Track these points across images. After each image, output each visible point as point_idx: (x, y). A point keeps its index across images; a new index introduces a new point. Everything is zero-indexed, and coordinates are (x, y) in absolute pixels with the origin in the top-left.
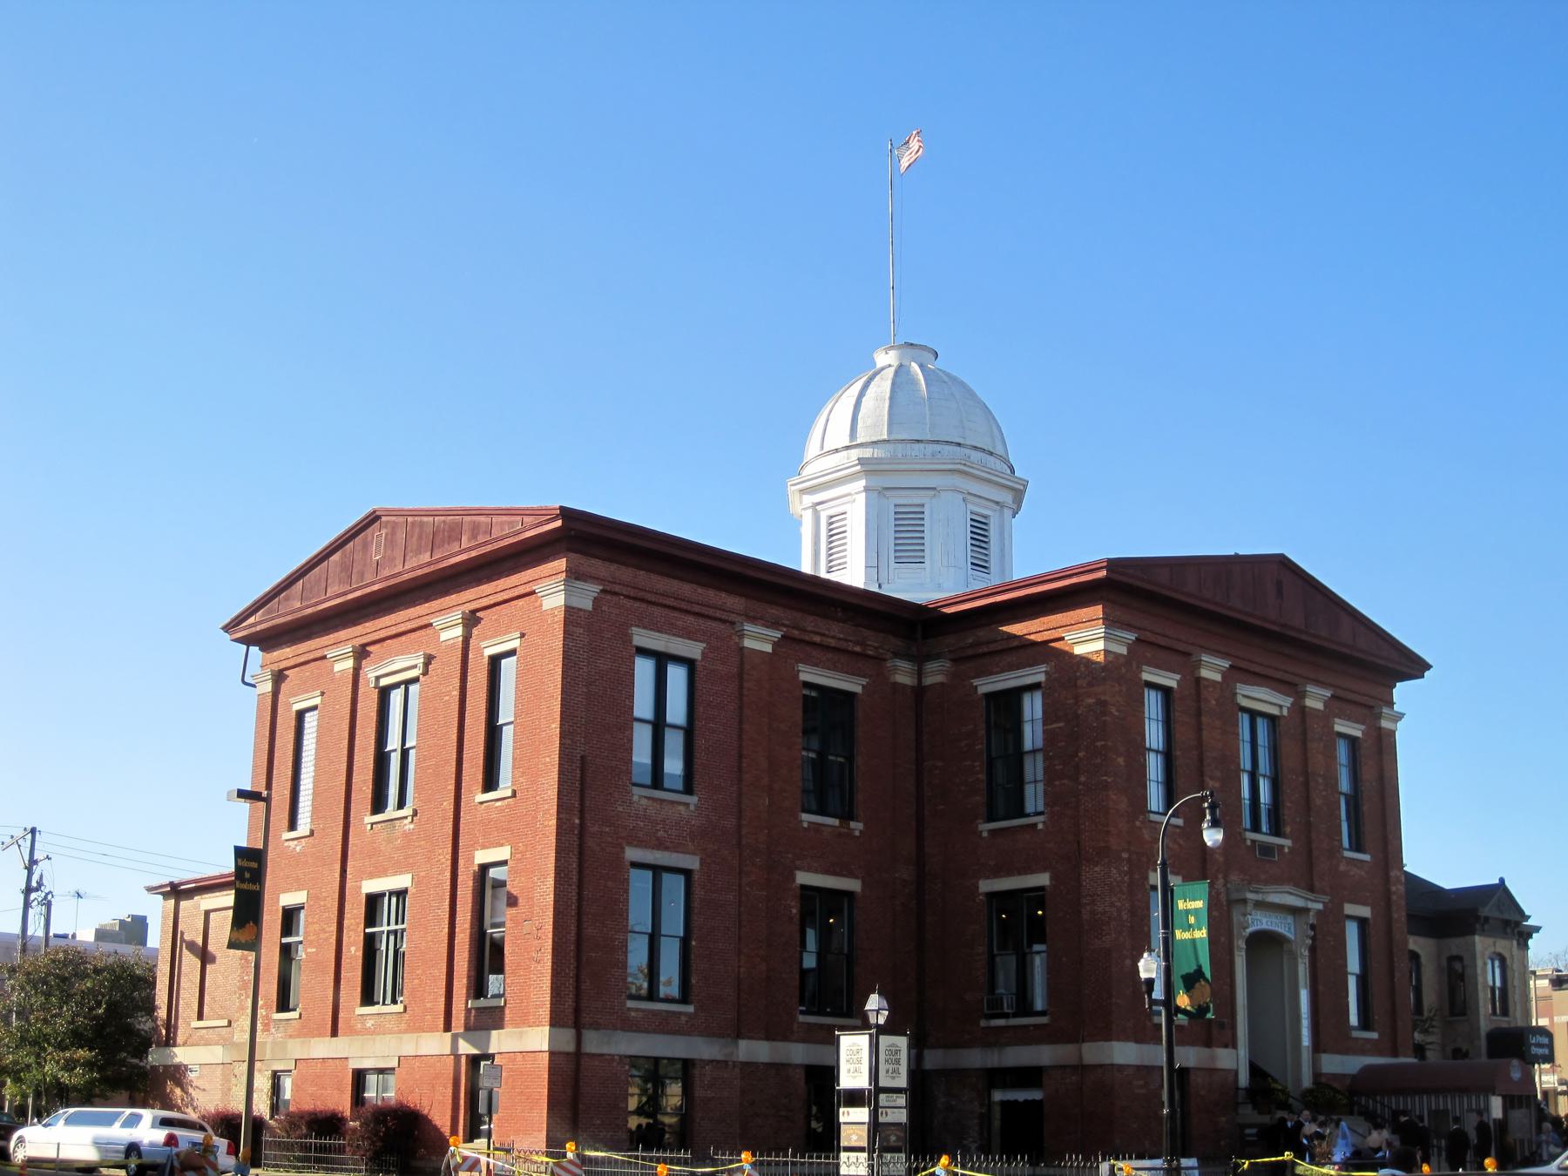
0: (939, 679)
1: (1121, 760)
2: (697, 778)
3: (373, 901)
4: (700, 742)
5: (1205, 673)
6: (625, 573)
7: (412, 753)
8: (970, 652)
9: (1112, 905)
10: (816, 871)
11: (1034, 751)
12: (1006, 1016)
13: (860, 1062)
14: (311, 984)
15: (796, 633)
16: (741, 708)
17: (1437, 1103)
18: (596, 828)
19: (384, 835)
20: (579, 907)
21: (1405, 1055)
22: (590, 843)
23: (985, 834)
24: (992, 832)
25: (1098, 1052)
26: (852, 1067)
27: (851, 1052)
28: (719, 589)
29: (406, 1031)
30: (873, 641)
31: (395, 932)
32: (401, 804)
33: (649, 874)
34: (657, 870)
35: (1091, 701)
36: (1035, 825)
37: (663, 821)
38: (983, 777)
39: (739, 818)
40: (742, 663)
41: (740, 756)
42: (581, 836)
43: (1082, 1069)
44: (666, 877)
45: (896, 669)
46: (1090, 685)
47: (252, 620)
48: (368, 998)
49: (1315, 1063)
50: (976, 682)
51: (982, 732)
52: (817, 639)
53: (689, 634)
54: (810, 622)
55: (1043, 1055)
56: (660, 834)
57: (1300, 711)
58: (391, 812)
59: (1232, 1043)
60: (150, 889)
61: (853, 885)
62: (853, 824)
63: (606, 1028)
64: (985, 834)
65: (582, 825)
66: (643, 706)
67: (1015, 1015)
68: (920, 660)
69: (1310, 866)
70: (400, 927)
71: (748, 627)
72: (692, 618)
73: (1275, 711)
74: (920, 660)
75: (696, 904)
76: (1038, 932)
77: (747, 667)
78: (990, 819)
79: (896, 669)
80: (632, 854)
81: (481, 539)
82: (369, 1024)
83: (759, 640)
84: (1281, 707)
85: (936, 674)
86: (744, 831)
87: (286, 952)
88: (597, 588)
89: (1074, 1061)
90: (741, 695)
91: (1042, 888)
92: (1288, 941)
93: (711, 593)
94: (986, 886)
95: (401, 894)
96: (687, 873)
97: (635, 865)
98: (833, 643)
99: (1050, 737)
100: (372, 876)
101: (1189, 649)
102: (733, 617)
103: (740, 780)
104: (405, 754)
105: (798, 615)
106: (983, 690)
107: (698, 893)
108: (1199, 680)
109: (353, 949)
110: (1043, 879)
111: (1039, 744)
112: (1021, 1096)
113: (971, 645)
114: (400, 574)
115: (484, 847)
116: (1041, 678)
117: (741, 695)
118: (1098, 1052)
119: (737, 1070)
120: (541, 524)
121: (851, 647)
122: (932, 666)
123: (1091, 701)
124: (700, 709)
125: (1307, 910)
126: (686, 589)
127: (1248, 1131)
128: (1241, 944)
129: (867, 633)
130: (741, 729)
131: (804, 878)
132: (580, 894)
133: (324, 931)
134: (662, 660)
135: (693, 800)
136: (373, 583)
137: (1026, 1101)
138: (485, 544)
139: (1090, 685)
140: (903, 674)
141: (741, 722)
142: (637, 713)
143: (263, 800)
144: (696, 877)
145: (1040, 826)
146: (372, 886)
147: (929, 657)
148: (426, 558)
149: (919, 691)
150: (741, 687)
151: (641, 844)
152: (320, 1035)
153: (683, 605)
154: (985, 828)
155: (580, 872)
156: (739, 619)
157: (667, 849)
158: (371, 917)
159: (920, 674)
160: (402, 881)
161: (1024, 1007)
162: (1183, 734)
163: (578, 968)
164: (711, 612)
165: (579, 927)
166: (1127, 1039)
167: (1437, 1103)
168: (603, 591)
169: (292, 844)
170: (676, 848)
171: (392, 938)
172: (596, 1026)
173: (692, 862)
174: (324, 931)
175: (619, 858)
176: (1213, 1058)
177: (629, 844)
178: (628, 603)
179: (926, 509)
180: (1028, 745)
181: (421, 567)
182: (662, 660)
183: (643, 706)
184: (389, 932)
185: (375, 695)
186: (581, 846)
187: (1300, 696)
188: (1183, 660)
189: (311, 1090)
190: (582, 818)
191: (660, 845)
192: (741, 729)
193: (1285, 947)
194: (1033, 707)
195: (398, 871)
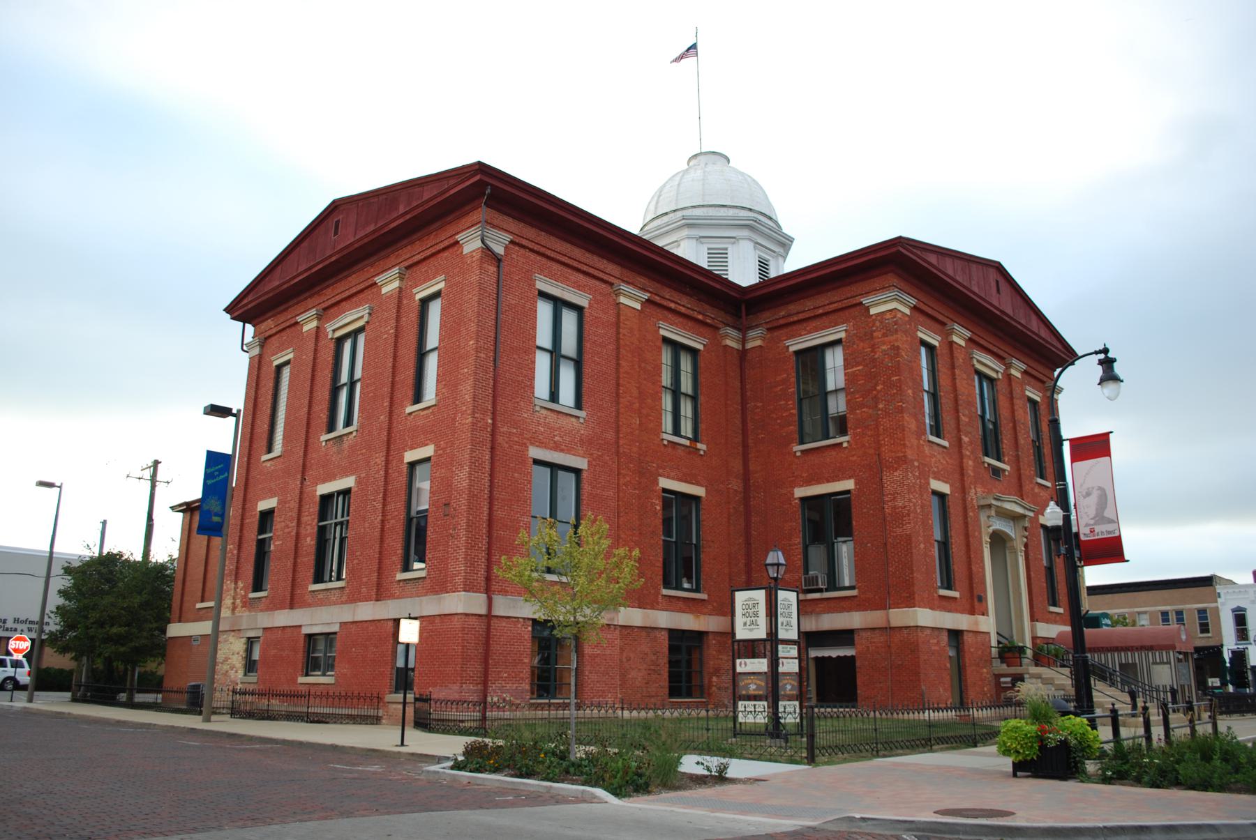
0: (758, 343)
1: (910, 392)
2: (585, 399)
3: (326, 499)
4: (587, 370)
5: (955, 339)
6: (530, 232)
7: (358, 386)
8: (782, 322)
9: (910, 501)
10: (673, 479)
11: (836, 391)
12: (820, 590)
13: (756, 615)
14: (276, 569)
15: (657, 299)
16: (618, 348)
17: (1127, 658)
18: (505, 429)
19: (334, 449)
20: (491, 492)
21: (1190, 610)
22: (500, 439)
23: (798, 454)
24: (802, 451)
25: (900, 616)
26: (748, 620)
27: (746, 606)
28: (603, 257)
29: (346, 602)
30: (712, 314)
31: (341, 523)
32: (348, 422)
33: (548, 470)
34: (554, 467)
35: (884, 347)
36: (841, 444)
37: (559, 428)
38: (795, 411)
39: (618, 432)
40: (618, 315)
41: (618, 385)
42: (493, 434)
43: (889, 630)
44: (561, 474)
45: (727, 335)
46: (885, 335)
47: (245, 301)
48: (319, 579)
49: (1033, 630)
50: (788, 343)
51: (794, 380)
52: (672, 305)
53: (578, 286)
54: (667, 293)
55: (853, 620)
56: (557, 438)
57: (1009, 377)
58: (340, 429)
59: (984, 613)
60: (172, 508)
61: (699, 491)
62: (699, 446)
63: (512, 594)
64: (798, 454)
65: (494, 424)
66: (544, 337)
67: (827, 590)
68: (743, 330)
69: (1021, 486)
70: (346, 518)
71: (624, 287)
72: (581, 276)
73: (994, 375)
74: (743, 330)
75: (584, 497)
76: (845, 529)
77: (622, 318)
78: (802, 443)
79: (727, 335)
80: (535, 452)
81: (414, 204)
82: (320, 596)
83: (631, 298)
84: (997, 372)
85: (755, 340)
86: (621, 442)
87: (262, 545)
88: (509, 237)
89: (882, 624)
90: (618, 339)
91: (848, 492)
92: (1011, 539)
93: (596, 258)
94: (800, 492)
95: (346, 492)
96: (577, 472)
97: (537, 462)
98: (683, 310)
99: (850, 379)
100: (324, 481)
101: (945, 320)
102: (611, 279)
103: (618, 403)
104: (352, 384)
105: (658, 285)
106: (792, 349)
107: (586, 487)
108: (952, 343)
109: (309, 539)
110: (849, 484)
111: (841, 384)
112: (834, 653)
113: (784, 317)
114: (352, 244)
115: (412, 448)
116: (842, 335)
117: (618, 339)
118: (900, 616)
119: (617, 632)
120: (463, 182)
121: (695, 315)
122: (751, 334)
123: (884, 347)
124: (587, 345)
125: (1024, 516)
126: (577, 253)
127: (1002, 680)
128: (986, 539)
129: (707, 307)
130: (618, 364)
131: (665, 483)
132: (491, 481)
133: (287, 526)
134: (559, 304)
135: (582, 414)
136: (331, 256)
137: (838, 657)
138: (417, 207)
139: (885, 335)
140: (731, 340)
141: (618, 359)
142: (539, 342)
143: (234, 415)
144: (585, 475)
145: (845, 445)
146: (324, 489)
147: (751, 328)
148: (372, 228)
149: (743, 353)
150: (618, 333)
151: (542, 445)
152: (281, 608)
153: (575, 264)
154: (798, 448)
155: (492, 463)
156: (615, 281)
157: (562, 451)
158: (323, 515)
159: (744, 341)
160: (348, 482)
161: (833, 584)
162: (944, 381)
163: (489, 543)
164: (596, 273)
165: (490, 509)
166: (924, 607)
167: (1127, 658)
168: (512, 242)
169: (268, 464)
170: (569, 450)
171: (338, 528)
172: (504, 592)
173: (581, 463)
174: (287, 526)
175: (522, 457)
176: (977, 623)
177: (532, 444)
178: (533, 256)
179: (729, 251)
180: (831, 386)
181: (366, 236)
182: (559, 304)
183: (544, 337)
184: (336, 524)
185: (332, 346)
186: (493, 441)
187: (1008, 366)
188: (939, 324)
189: (273, 652)
190: (494, 419)
191: (557, 447)
192: (618, 364)
193: (1008, 545)
194: (835, 361)
195: (345, 474)
